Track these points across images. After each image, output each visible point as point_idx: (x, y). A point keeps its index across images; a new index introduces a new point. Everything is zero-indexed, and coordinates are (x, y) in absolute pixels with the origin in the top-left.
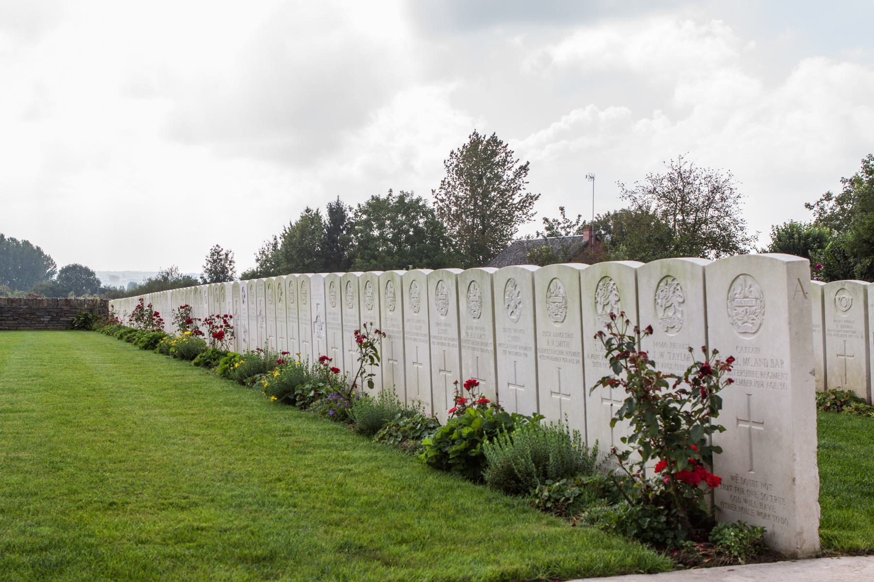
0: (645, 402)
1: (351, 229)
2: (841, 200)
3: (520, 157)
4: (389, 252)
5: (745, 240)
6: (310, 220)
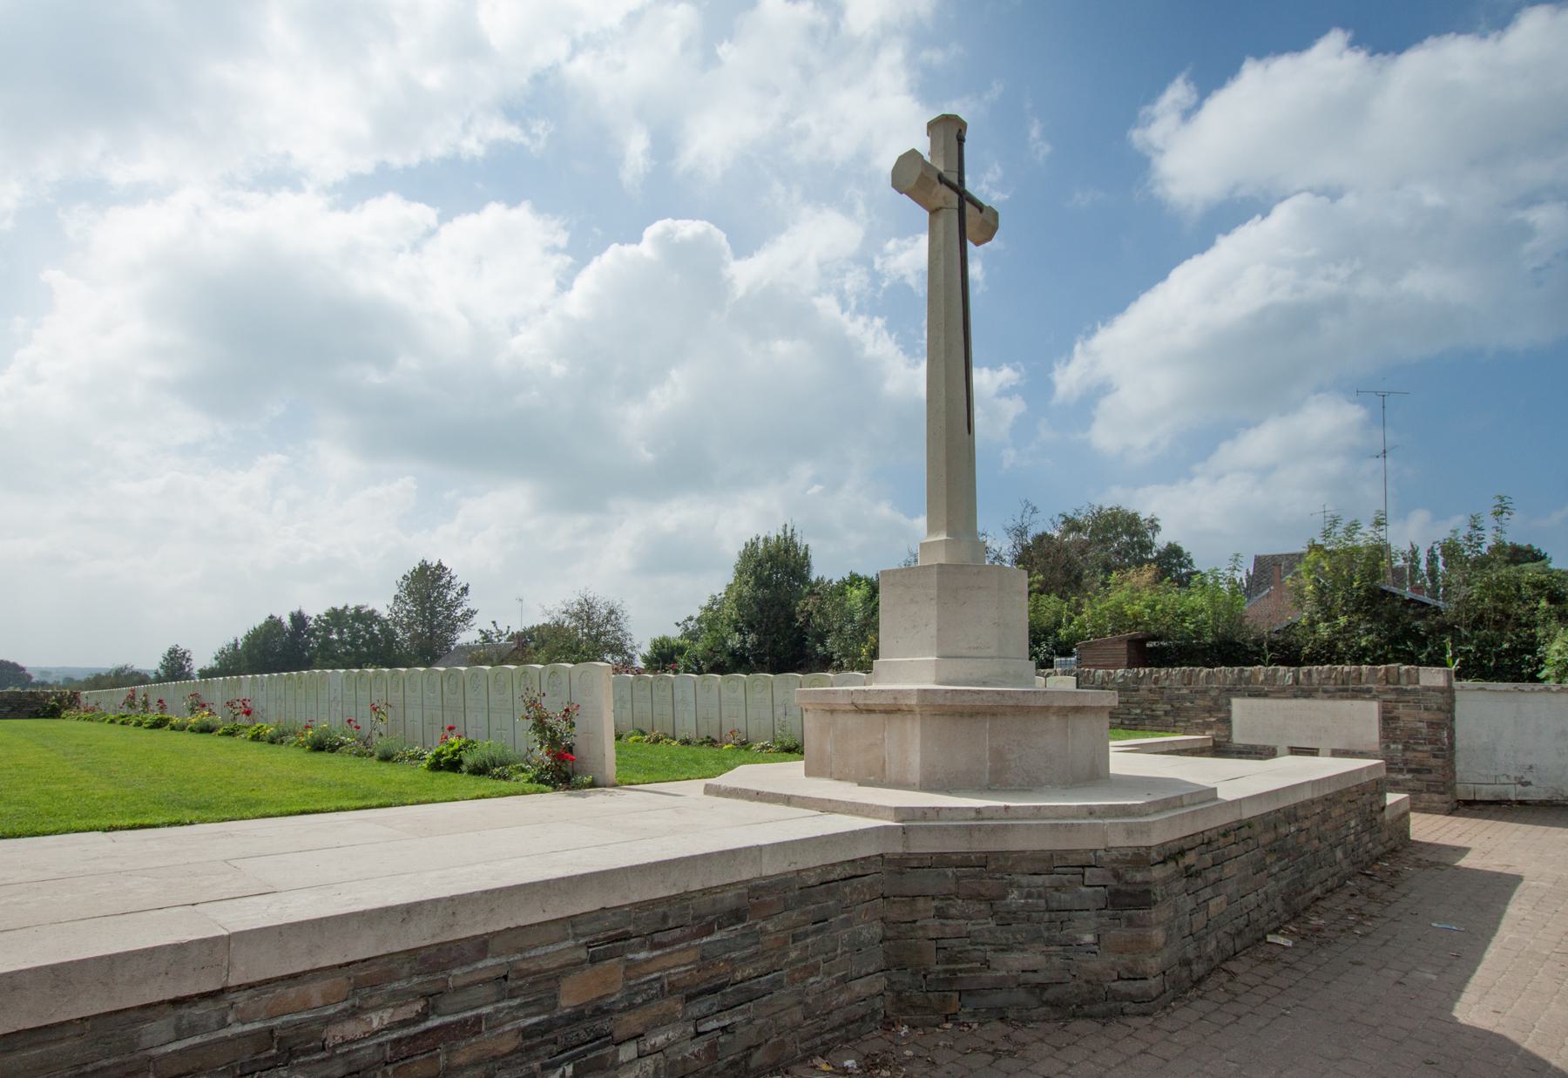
0: (541, 725)
1: (312, 633)
2: (699, 621)
3: (460, 581)
4: (347, 653)
5: (633, 648)
6: (273, 624)
